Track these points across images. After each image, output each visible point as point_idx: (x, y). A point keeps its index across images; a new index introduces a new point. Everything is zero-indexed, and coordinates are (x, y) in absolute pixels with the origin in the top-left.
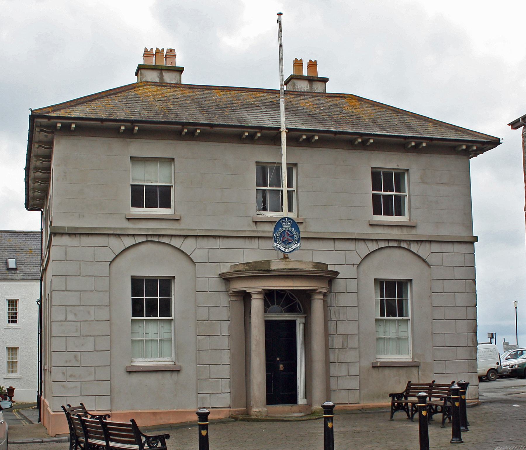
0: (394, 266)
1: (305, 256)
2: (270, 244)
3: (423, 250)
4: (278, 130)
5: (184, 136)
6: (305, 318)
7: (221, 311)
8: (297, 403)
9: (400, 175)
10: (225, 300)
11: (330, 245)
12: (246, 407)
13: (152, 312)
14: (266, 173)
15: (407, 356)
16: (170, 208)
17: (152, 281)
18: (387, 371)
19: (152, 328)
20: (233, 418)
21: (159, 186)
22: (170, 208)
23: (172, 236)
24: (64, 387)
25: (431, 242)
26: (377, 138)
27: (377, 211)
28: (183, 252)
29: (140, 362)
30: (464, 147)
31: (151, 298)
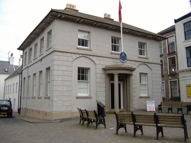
1: (127, 64)
2: (119, 61)
3: (94, 59)
4: (120, 27)
5: (58, 18)
6: (123, 83)
10: (104, 76)
11: (102, 58)
14: (115, 41)
15: (146, 95)
18: (143, 99)
19: (83, 85)
21: (81, 39)
23: (90, 55)
24: (57, 103)
25: (152, 63)
26: (116, 27)
27: (79, 45)
28: (92, 60)
29: (80, 95)
30: (151, 37)
31: (83, 74)
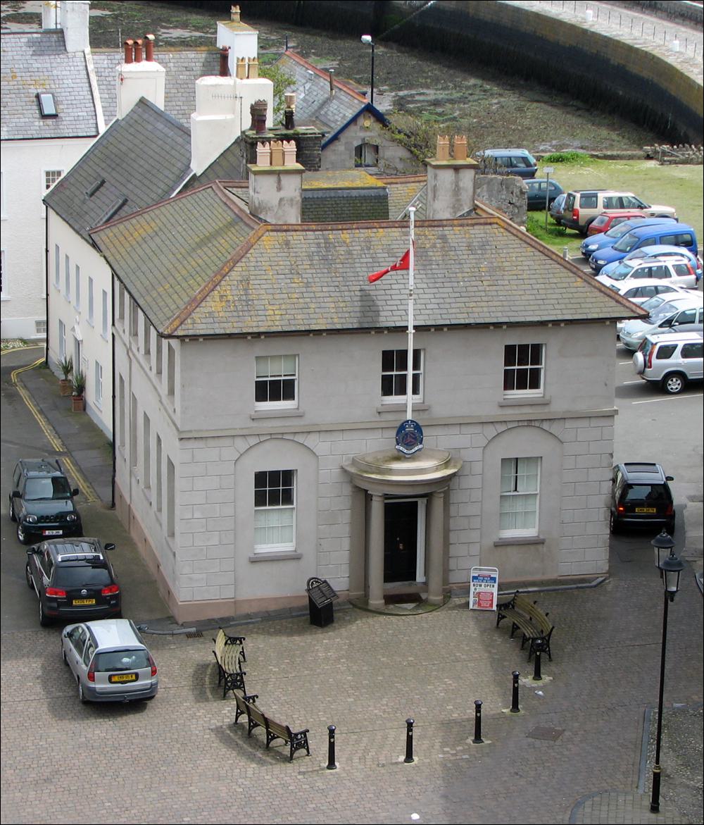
0: (522, 444)
7: (341, 505)
8: (415, 580)
9: (537, 349)
12: (365, 591)
13: (274, 501)
16: (294, 399)
17: (274, 474)
18: (509, 549)
19: (275, 515)
20: (351, 604)
22: (294, 399)
24: (191, 579)
29: (264, 549)
